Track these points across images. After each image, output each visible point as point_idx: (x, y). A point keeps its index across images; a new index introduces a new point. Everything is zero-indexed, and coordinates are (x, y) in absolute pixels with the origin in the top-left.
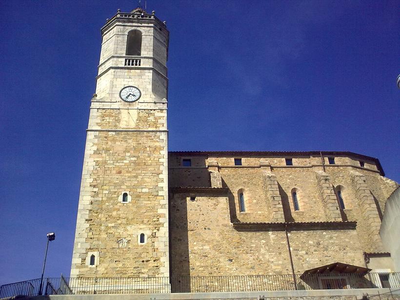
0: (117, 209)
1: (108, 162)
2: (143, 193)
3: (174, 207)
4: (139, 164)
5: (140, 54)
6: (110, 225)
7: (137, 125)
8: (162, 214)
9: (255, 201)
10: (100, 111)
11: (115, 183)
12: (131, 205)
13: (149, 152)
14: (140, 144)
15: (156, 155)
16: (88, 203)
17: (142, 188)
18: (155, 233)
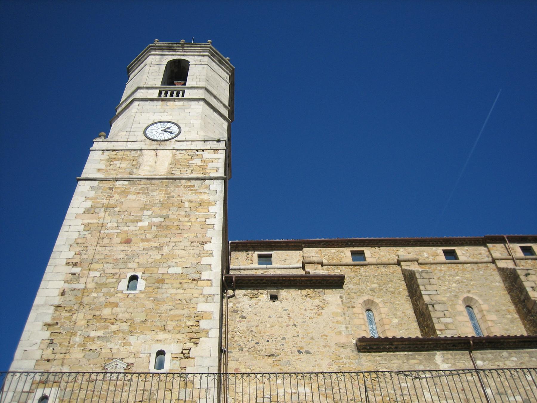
0: (113, 303)
1: (109, 225)
2: (170, 275)
3: (234, 311)
4: (167, 228)
5: (185, 84)
6: (93, 334)
7: (171, 170)
8: (206, 312)
9: (395, 321)
10: (106, 153)
11: (116, 259)
12: (143, 295)
13: (188, 209)
14: (173, 197)
15: (201, 213)
16: (57, 292)
17: (169, 267)
18: (189, 349)
